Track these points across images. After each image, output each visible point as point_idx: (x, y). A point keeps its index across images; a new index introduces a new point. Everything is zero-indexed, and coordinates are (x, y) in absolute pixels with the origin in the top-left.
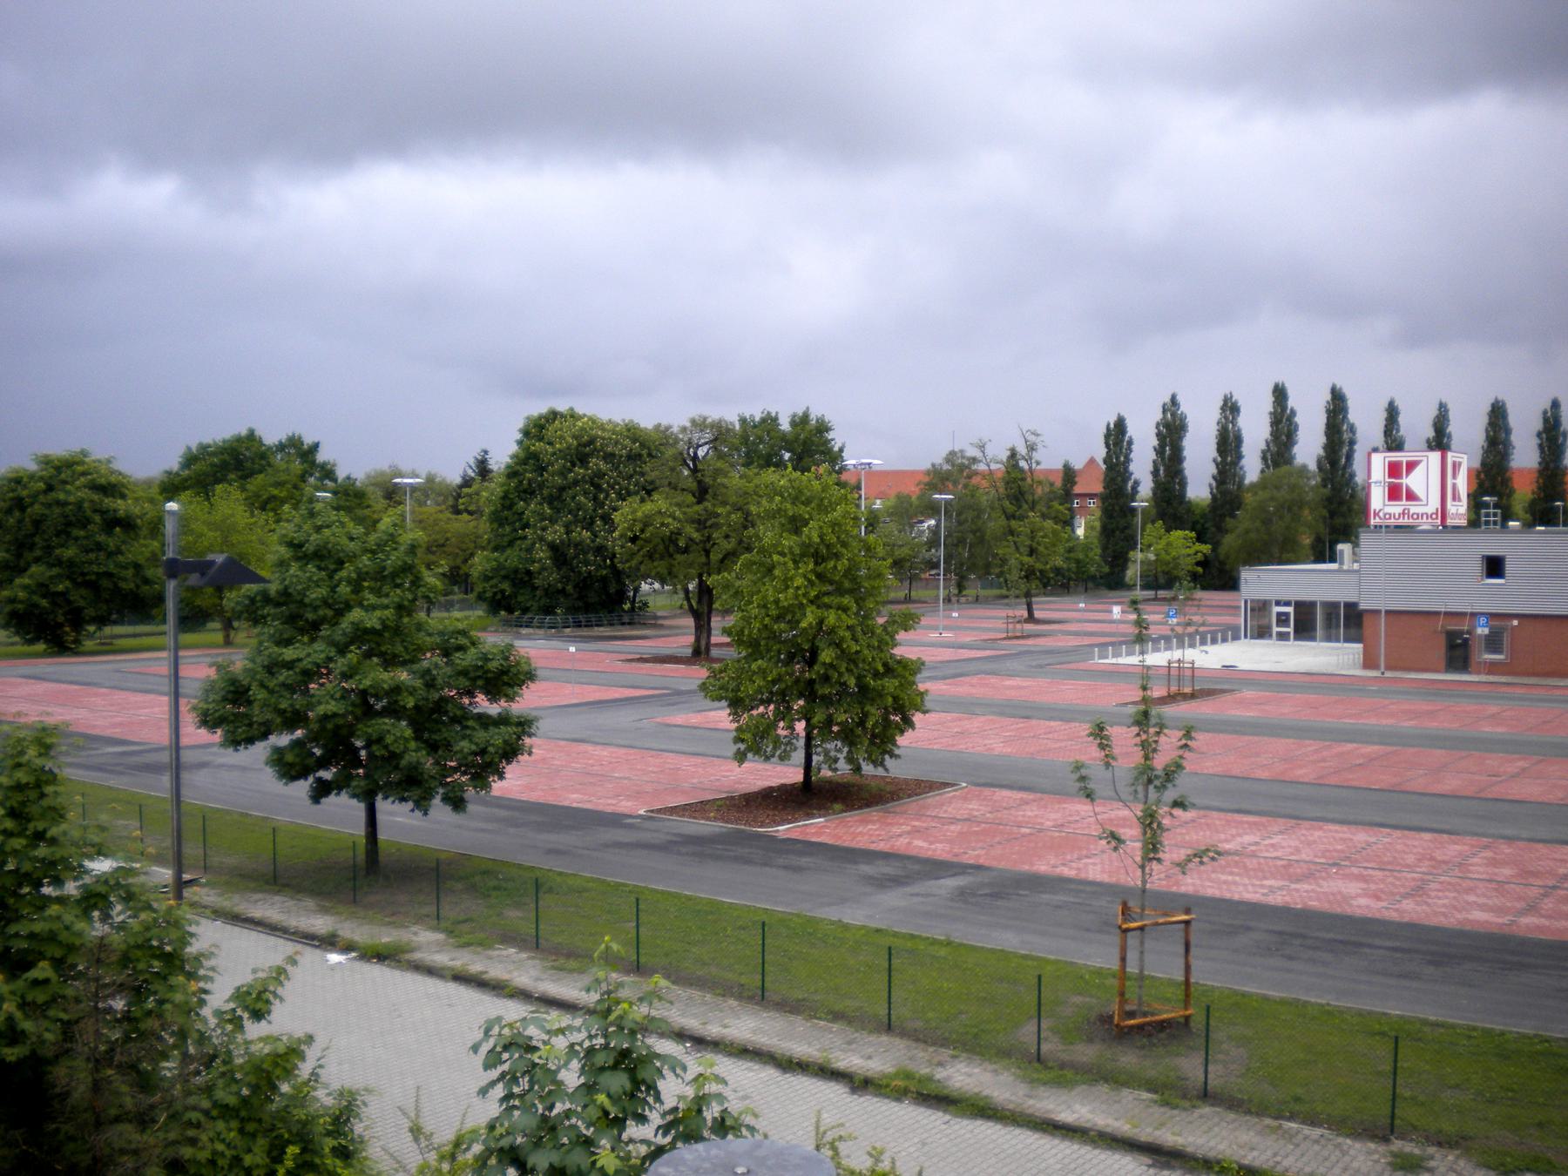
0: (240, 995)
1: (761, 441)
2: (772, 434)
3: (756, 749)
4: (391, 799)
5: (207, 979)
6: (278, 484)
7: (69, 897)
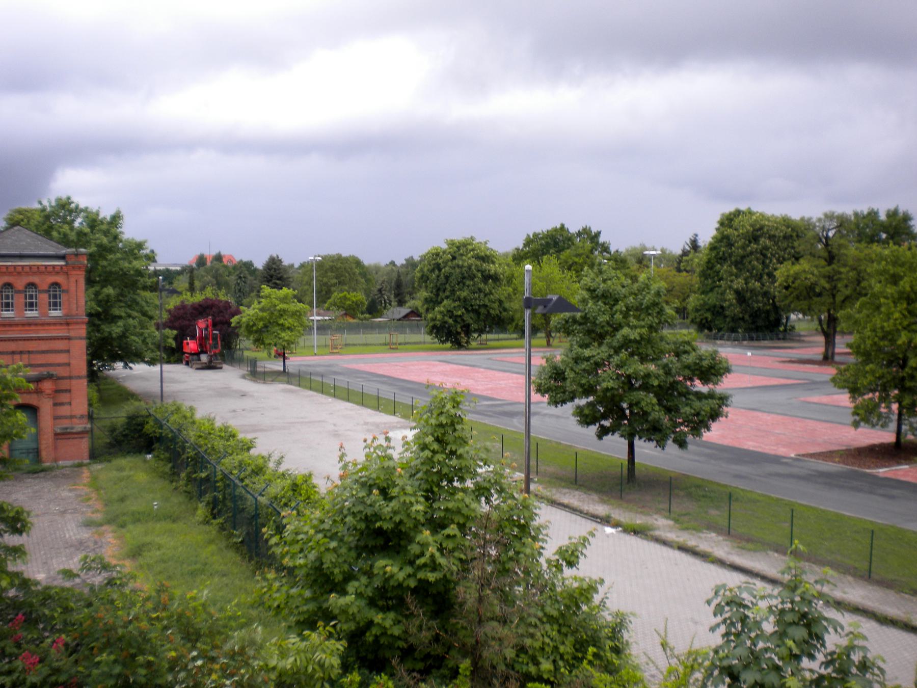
0: (561, 552)
1: (868, 226)
2: (875, 222)
3: (867, 420)
4: (643, 439)
5: (544, 541)
6: (578, 255)
7: (468, 488)
